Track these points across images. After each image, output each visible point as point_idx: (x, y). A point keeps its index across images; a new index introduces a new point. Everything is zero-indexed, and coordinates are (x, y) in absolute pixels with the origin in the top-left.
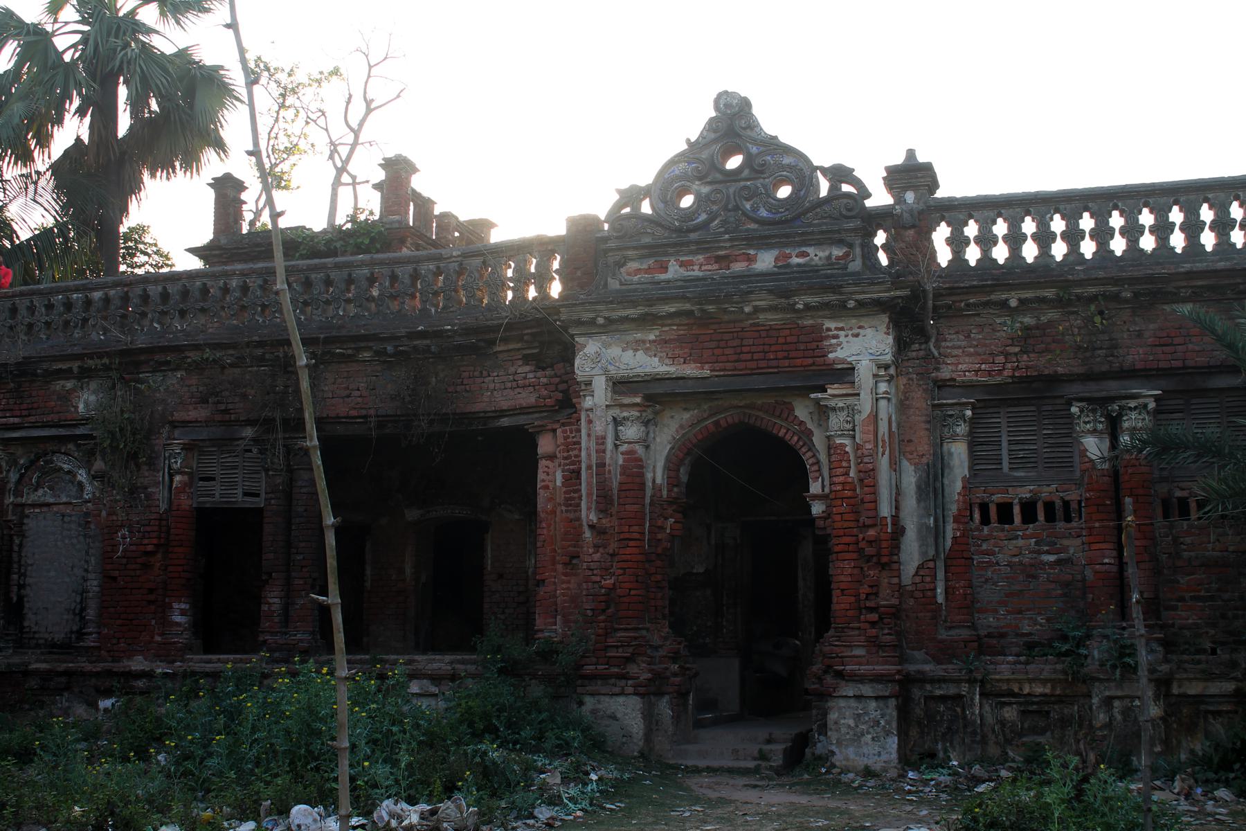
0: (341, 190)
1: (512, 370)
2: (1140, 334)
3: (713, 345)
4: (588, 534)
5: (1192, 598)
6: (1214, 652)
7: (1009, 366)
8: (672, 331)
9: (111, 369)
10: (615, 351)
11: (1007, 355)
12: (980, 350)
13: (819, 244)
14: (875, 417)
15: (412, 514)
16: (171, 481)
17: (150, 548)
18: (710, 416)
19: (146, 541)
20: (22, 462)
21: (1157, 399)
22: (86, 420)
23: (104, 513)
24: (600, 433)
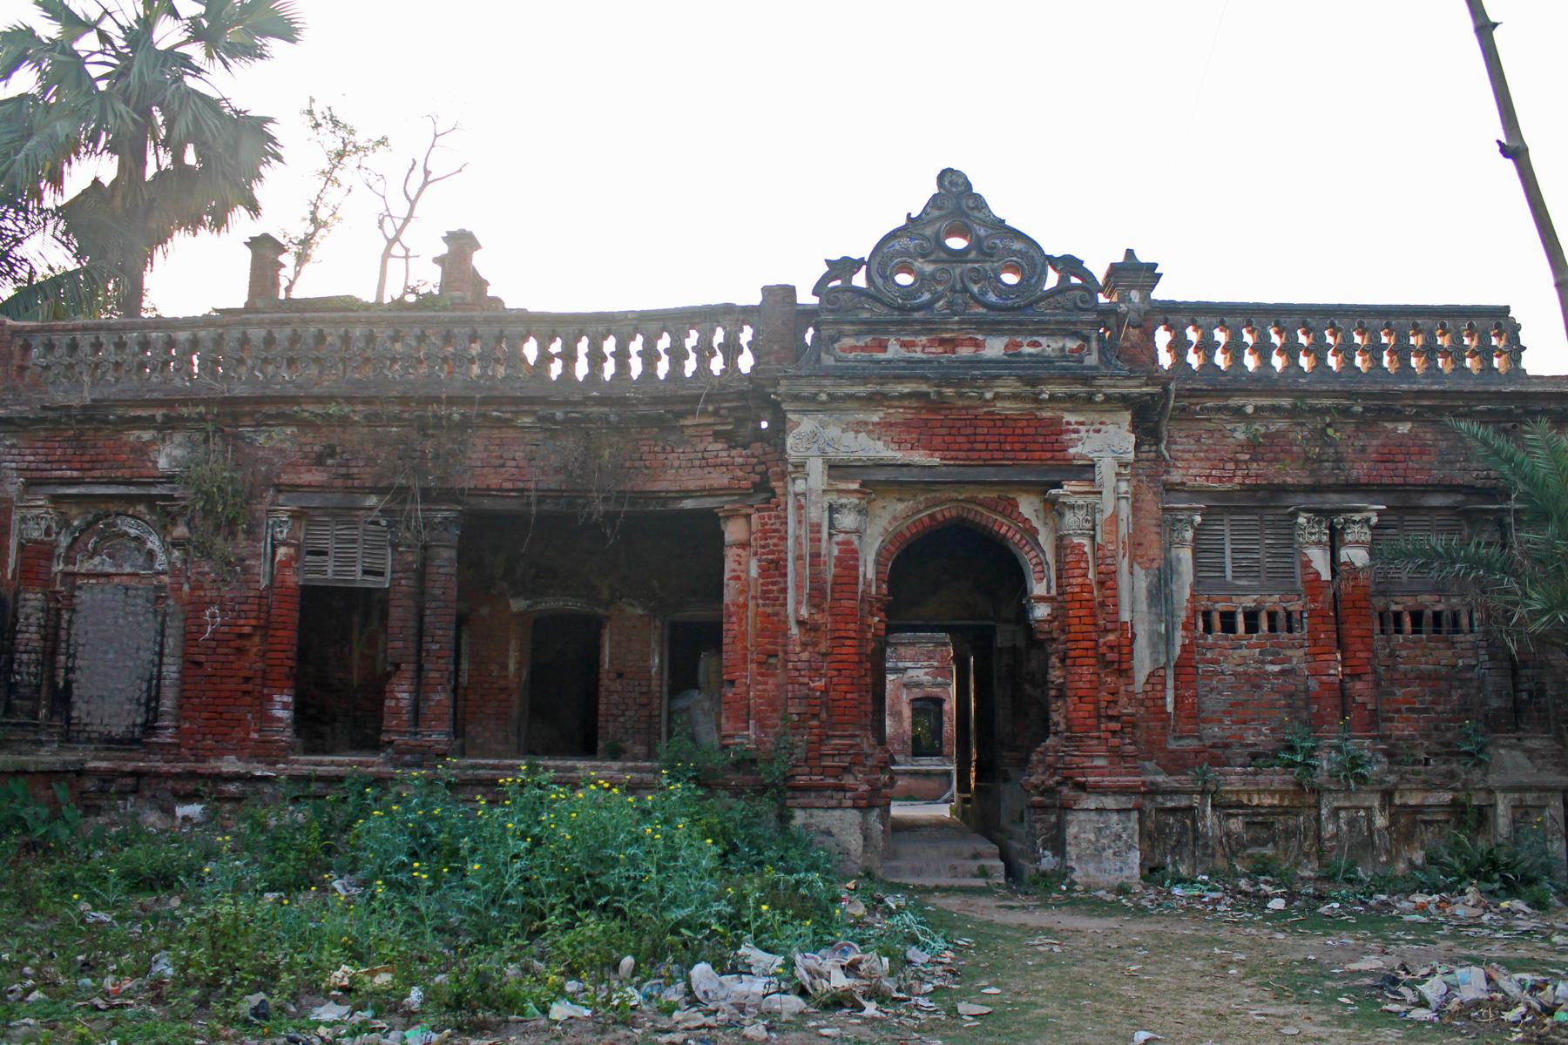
0: (390, 261)
1: (700, 447)
2: (1363, 450)
3: (943, 431)
4: (794, 630)
5: (1408, 710)
6: (1427, 763)
7: (1239, 473)
8: (898, 414)
9: (205, 420)
10: (833, 431)
11: (1237, 462)
12: (1212, 455)
13: (1052, 334)
14: (1115, 517)
15: (517, 605)
16: (274, 553)
17: (247, 630)
18: (927, 508)
19: (242, 622)
20: (76, 523)
21: (1380, 513)
22: (170, 479)
23: (186, 587)
24: (815, 520)
